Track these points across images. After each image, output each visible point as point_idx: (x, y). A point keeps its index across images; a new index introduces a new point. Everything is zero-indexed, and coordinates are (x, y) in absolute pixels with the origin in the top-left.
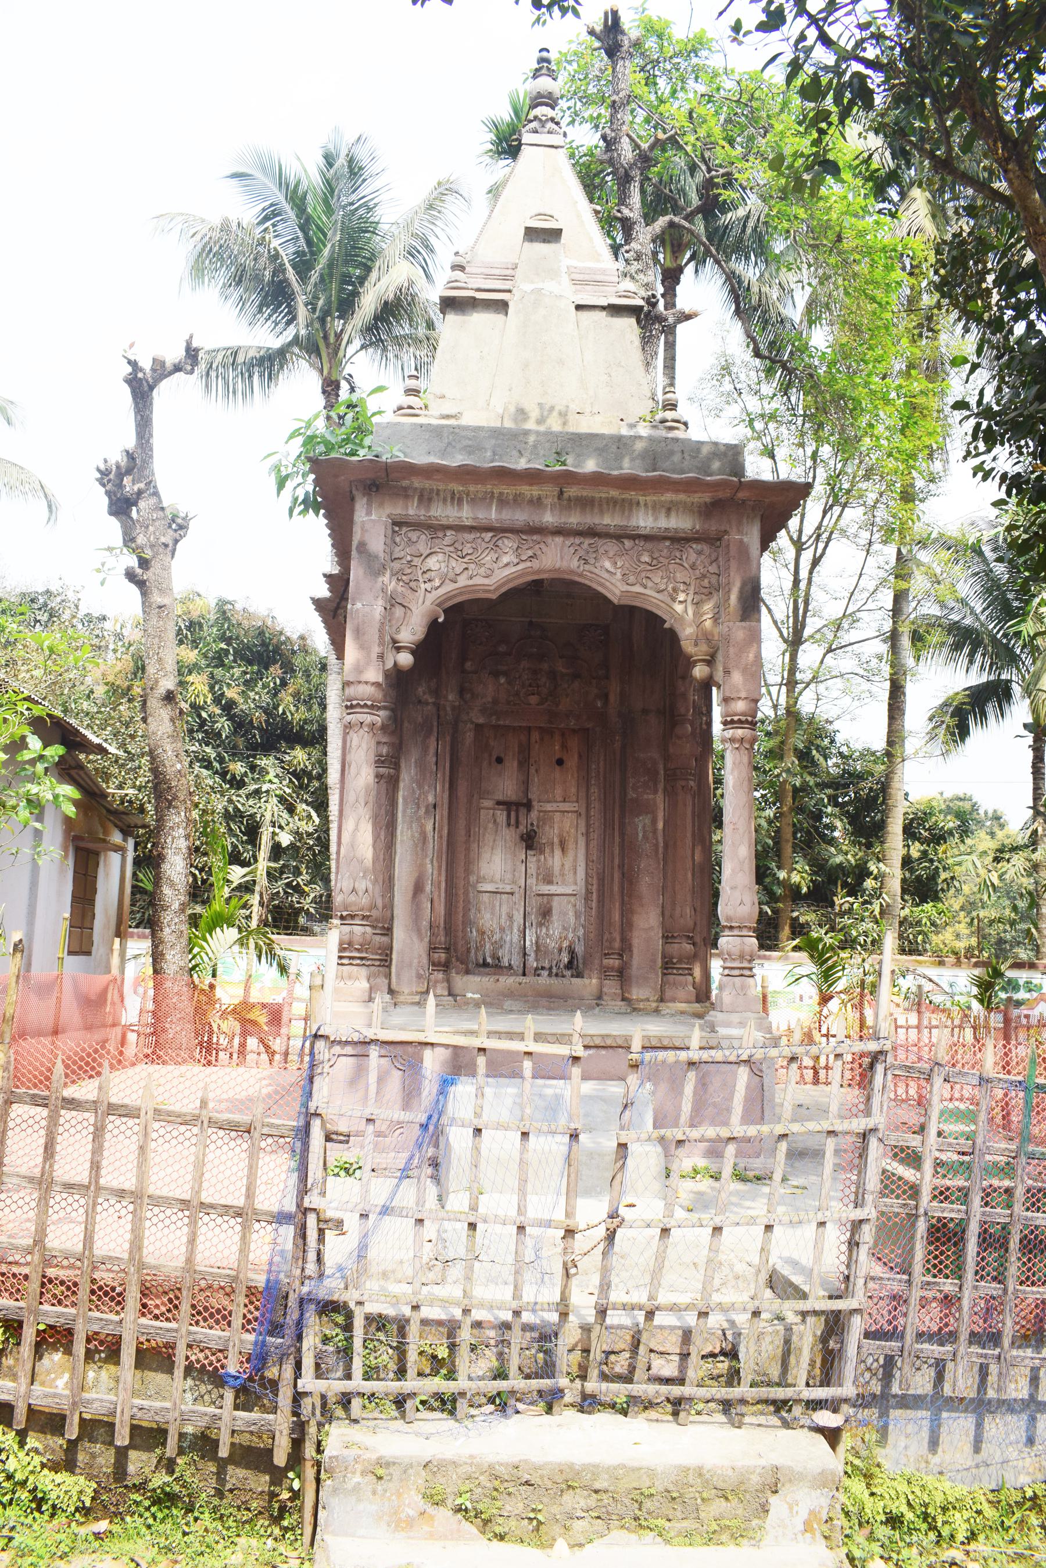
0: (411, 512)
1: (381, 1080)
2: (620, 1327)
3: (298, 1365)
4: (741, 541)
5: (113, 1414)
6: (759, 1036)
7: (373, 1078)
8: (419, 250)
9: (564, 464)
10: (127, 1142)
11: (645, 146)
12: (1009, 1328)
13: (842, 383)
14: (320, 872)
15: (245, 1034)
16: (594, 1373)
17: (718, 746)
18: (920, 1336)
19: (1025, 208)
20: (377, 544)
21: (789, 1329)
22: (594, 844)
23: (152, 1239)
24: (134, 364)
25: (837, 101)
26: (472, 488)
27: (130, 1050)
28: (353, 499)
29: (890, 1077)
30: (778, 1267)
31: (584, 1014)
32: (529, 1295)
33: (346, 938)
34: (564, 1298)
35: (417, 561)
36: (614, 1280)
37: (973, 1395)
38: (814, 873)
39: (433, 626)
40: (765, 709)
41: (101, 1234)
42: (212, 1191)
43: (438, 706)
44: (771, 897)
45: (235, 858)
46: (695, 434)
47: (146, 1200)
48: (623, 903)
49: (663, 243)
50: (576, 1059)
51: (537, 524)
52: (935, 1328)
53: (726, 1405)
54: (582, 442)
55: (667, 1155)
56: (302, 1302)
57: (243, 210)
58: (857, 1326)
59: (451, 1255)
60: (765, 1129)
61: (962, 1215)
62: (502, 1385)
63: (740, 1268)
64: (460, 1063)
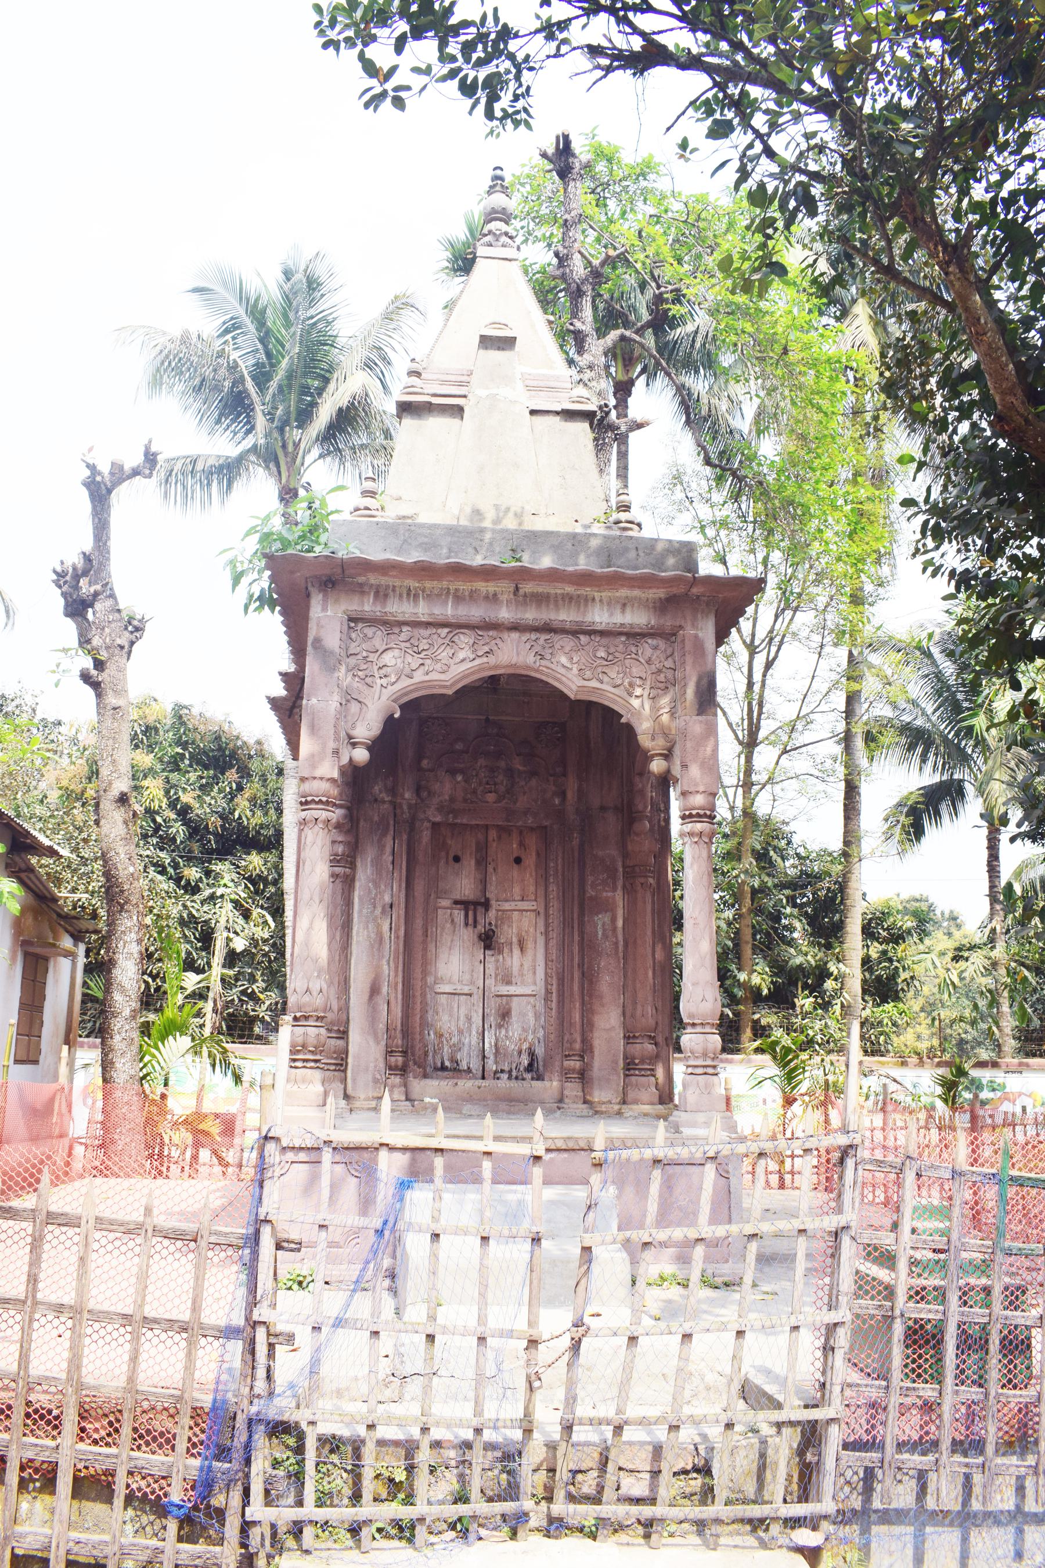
0: (367, 608)
1: (334, 1187)
2: (587, 1444)
3: (246, 1492)
4: (696, 636)
5: (48, 1548)
6: (724, 1135)
7: (325, 1181)
8: (376, 362)
9: (519, 560)
10: (67, 1253)
11: (596, 262)
12: (992, 1433)
13: (791, 489)
14: (276, 979)
15: (197, 1145)
16: (560, 1494)
17: (676, 846)
18: (900, 1446)
19: (967, 309)
20: (332, 639)
21: (764, 1442)
22: (553, 943)
23: (92, 1357)
24: (92, 467)
25: (783, 207)
26: (428, 584)
27: (77, 1165)
28: (308, 596)
29: (860, 1172)
30: (750, 1377)
31: (548, 1113)
32: (490, 1412)
33: (300, 1040)
34: (527, 1414)
35: (372, 657)
36: (581, 1394)
37: (959, 1508)
38: (775, 975)
39: (390, 723)
40: (722, 811)
41: (38, 1352)
42: (155, 1304)
43: (395, 805)
44: (731, 999)
45: (189, 965)
46: (648, 532)
47: (86, 1315)
48: (583, 1004)
49: (615, 357)
50: (537, 1158)
51: (494, 620)
52: (915, 1437)
53: (701, 1525)
54: (535, 538)
55: (634, 1262)
56: (250, 1422)
57: (205, 324)
58: (834, 1437)
59: (408, 1370)
60: (734, 1228)
61: (939, 1316)
62: (463, 1509)
63: (711, 1378)
64: (419, 1162)
